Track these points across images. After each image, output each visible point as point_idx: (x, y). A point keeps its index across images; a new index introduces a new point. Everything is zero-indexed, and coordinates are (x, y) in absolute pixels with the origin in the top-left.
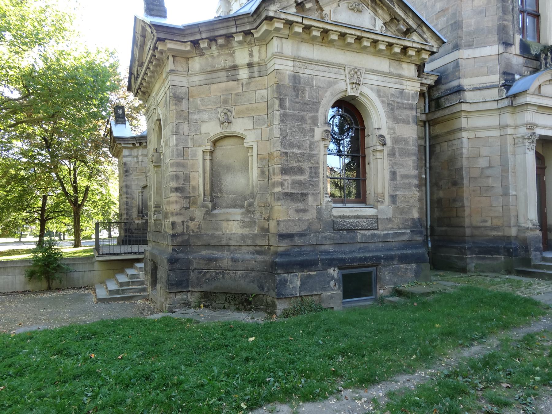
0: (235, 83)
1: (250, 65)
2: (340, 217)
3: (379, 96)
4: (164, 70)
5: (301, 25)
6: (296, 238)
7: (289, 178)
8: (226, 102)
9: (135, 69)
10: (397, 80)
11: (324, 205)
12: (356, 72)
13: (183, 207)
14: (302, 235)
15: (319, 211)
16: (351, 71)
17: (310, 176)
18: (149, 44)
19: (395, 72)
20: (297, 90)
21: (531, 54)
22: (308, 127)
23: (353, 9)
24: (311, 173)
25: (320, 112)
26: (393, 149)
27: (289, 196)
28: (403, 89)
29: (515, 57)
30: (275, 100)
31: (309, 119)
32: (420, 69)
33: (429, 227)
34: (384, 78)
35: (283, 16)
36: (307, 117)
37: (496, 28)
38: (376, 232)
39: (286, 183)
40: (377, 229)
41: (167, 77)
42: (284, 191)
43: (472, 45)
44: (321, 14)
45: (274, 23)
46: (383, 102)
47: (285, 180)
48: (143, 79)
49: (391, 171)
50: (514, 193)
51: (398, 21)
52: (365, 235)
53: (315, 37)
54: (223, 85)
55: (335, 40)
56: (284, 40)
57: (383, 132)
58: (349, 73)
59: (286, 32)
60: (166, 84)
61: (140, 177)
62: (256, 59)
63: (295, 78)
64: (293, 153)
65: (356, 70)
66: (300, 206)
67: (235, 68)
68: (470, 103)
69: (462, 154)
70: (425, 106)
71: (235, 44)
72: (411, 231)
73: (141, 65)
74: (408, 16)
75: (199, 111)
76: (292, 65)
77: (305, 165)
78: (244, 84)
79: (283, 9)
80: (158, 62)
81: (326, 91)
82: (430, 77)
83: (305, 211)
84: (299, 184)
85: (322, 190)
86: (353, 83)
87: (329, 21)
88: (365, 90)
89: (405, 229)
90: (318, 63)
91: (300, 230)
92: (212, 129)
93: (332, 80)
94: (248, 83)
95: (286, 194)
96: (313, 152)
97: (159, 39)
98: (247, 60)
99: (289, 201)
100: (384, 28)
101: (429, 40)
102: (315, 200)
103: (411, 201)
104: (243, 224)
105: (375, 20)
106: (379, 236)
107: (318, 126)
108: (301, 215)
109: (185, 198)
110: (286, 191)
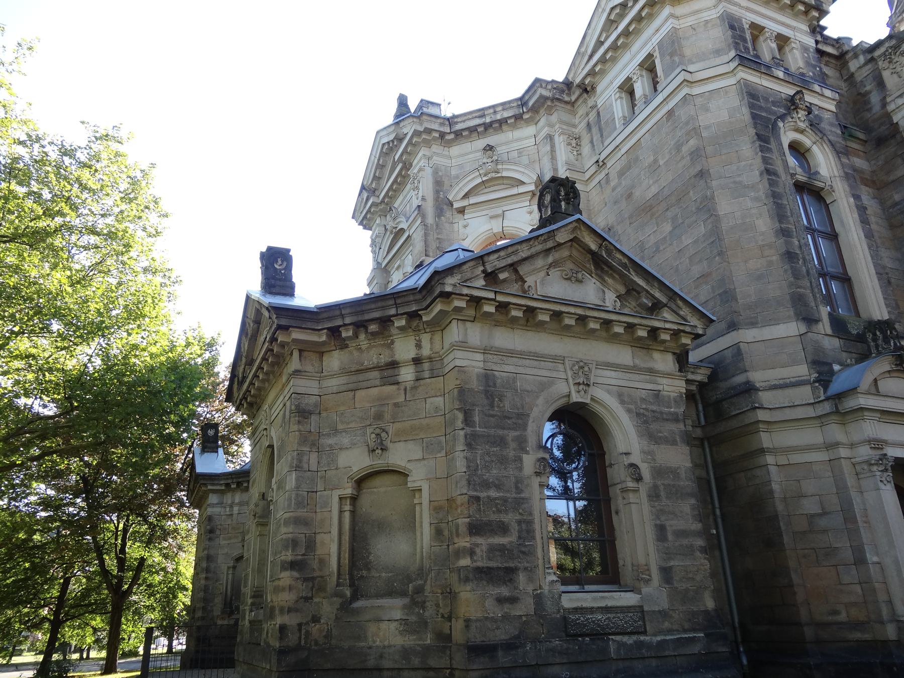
0: (394, 387)
1: (417, 361)
2: (576, 610)
3: (622, 402)
4: (285, 370)
6: (500, 653)
7: (483, 542)
8: (379, 416)
9: (241, 369)
11: (546, 588)
12: (582, 368)
13: (302, 598)
14: (510, 646)
15: (539, 599)
16: (574, 365)
17: (520, 538)
19: (643, 365)
20: (491, 396)
21: (850, 333)
22: (512, 454)
24: (520, 532)
25: (530, 429)
26: (655, 487)
27: (484, 575)
29: (827, 338)
30: (457, 412)
31: (512, 440)
32: (682, 359)
33: (737, 625)
34: (628, 375)
35: (466, 291)
36: (509, 439)
37: (788, 297)
38: (642, 638)
39: (478, 550)
40: (645, 633)
41: (288, 381)
42: (475, 564)
43: (757, 323)
45: (452, 300)
46: (629, 411)
47: (477, 545)
48: (251, 383)
49: (656, 525)
50: (875, 559)
51: (639, 293)
52: (624, 644)
54: (374, 391)
55: (545, 322)
56: (468, 324)
57: (635, 458)
58: (571, 369)
59: (472, 312)
61: (233, 541)
62: (426, 352)
63: (488, 378)
64: (489, 497)
65: (582, 364)
66: (505, 591)
67: (394, 365)
68: (770, 409)
69: (771, 492)
70: (698, 415)
71: (394, 331)
72: (707, 635)
73: (250, 363)
74: (652, 286)
75: (336, 431)
77: (510, 518)
78: (408, 388)
79: (465, 281)
81: (538, 397)
83: (513, 600)
84: (500, 551)
85: (540, 562)
86: (579, 384)
88: (600, 393)
89: (694, 630)
91: (507, 637)
92: (355, 460)
94: (414, 388)
95: (479, 570)
96: (522, 495)
97: (280, 327)
98: (412, 353)
99: (485, 583)
100: (618, 304)
101: (688, 318)
102: (531, 580)
103: (699, 578)
104: (407, 627)
105: (604, 292)
106: (649, 646)
107: (527, 453)
108: (507, 608)
109: (306, 580)
110: (480, 564)
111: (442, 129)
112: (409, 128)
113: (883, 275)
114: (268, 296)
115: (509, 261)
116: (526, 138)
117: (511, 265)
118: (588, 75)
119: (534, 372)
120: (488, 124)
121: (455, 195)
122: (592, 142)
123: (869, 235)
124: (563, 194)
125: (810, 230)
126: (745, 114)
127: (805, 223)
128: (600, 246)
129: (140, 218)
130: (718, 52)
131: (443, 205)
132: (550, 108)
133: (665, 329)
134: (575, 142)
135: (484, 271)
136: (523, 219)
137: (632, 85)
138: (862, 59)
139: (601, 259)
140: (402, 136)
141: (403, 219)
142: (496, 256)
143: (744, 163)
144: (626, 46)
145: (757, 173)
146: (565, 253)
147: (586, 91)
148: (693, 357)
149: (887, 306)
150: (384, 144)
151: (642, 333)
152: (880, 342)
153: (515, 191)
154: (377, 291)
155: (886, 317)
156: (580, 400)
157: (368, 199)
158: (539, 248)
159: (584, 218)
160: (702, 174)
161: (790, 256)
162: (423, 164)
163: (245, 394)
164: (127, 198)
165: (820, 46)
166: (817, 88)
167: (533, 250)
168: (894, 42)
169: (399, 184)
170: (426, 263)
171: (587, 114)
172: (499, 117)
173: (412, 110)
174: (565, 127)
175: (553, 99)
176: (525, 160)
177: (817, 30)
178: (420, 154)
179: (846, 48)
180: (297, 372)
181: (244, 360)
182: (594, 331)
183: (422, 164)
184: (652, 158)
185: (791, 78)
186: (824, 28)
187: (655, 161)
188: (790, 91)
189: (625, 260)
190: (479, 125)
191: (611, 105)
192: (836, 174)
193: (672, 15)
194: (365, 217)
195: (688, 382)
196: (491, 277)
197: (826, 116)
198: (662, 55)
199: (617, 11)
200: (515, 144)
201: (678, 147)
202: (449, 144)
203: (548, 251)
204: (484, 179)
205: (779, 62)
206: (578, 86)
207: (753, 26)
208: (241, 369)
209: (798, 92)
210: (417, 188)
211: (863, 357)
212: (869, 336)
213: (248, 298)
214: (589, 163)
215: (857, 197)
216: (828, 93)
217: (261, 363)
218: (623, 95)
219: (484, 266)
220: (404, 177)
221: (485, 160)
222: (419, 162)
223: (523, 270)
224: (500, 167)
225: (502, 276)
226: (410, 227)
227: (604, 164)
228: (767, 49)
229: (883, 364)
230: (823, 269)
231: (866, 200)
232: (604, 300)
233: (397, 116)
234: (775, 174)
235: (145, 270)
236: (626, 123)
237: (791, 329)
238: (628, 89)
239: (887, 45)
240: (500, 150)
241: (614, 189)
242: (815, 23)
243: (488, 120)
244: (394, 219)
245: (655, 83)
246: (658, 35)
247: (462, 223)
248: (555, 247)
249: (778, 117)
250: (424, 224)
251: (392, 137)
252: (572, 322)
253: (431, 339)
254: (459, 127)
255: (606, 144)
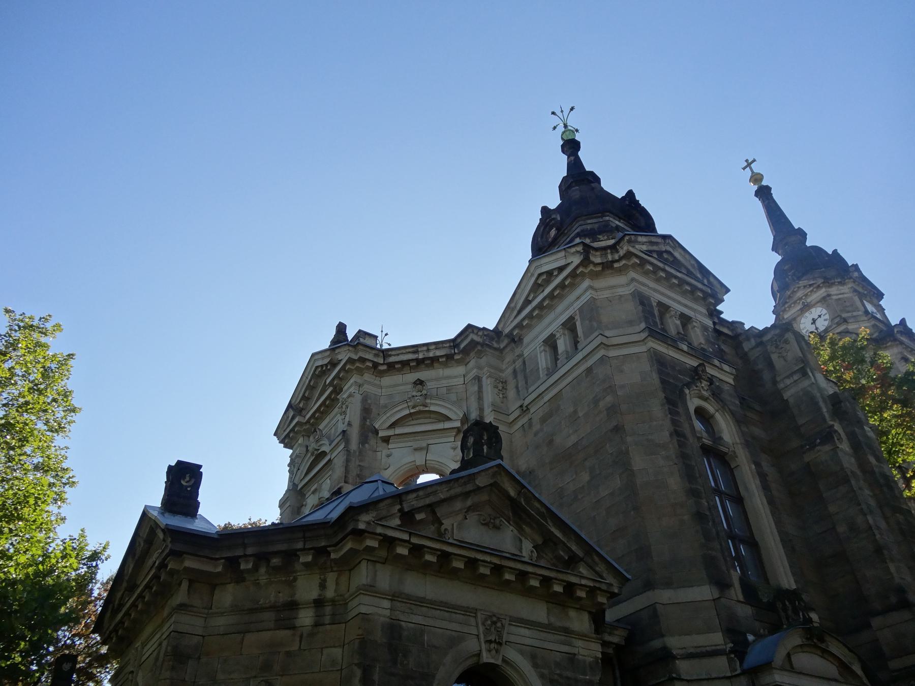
0: (288, 633)
1: (319, 603)
3: (535, 666)
4: (169, 602)
5: (407, 544)
8: (266, 667)
9: (119, 595)
10: (563, 638)
12: (494, 623)
16: (486, 620)
18: (156, 555)
19: (558, 624)
23: (486, 524)
28: (575, 654)
30: (355, 668)
32: (598, 619)
35: (379, 530)
41: (170, 615)
44: (439, 529)
46: (542, 676)
48: (127, 614)
53: (429, 563)
54: (266, 636)
55: (460, 569)
56: (378, 566)
58: (483, 624)
59: (383, 553)
60: (165, 629)
62: (330, 593)
63: (393, 629)
65: (495, 619)
67: (293, 606)
68: (688, 681)
71: (298, 567)
73: (132, 588)
76: (389, 606)
78: (305, 635)
79: (380, 519)
80: (162, 589)
82: (616, 632)
86: (490, 642)
87: (451, 541)
88: (512, 654)
90: (435, 604)
93: (453, 633)
94: (312, 635)
97: (173, 553)
98: (314, 594)
100: (535, 554)
105: (521, 541)
111: (375, 360)
112: (344, 355)
113: (786, 540)
114: (167, 515)
115: (428, 501)
116: (456, 377)
117: (429, 506)
118: (515, 328)
119: (444, 624)
120: (420, 358)
121: (381, 423)
122: (517, 387)
123: (771, 502)
124: (485, 438)
125: (717, 491)
126: (655, 379)
127: (713, 484)
128: (519, 493)
129: (45, 411)
130: (631, 323)
131: (368, 432)
132: (480, 352)
133: (581, 585)
134: (502, 385)
135: (400, 510)
136: (449, 454)
137: (555, 342)
138: (753, 342)
139: (518, 506)
140: (336, 362)
141: (326, 442)
142: (414, 495)
143: (655, 423)
144: (551, 307)
145: (667, 434)
146: (484, 497)
147: (513, 341)
148: (610, 616)
149: (794, 574)
150: (317, 367)
151: (558, 588)
152: (790, 612)
153: (440, 426)
154: (286, 522)
155: (794, 587)
156: (492, 661)
157: (293, 418)
158: (458, 490)
159: (506, 463)
160: (618, 429)
161: (700, 517)
162: (353, 390)
163: (117, 625)
164: (35, 389)
165: (717, 327)
166: (716, 362)
167: (452, 492)
168: (777, 331)
169: (327, 407)
170: (344, 491)
171: (514, 362)
172: (431, 354)
173: (350, 338)
174: (492, 371)
175: (483, 345)
176: (453, 397)
177: (715, 314)
178: (352, 381)
179: (739, 331)
180: (182, 607)
181: (125, 585)
182: (508, 582)
183: (352, 390)
184: (572, 409)
185: (694, 351)
186: (721, 313)
187: (575, 412)
188: (694, 363)
189: (543, 510)
190: (412, 360)
191: (536, 356)
192: (738, 441)
193: (591, 287)
194: (287, 436)
195: (605, 644)
196: (407, 517)
197: (726, 387)
198: (582, 319)
199: (544, 277)
200: (444, 381)
201: (596, 401)
202: (381, 374)
203: (467, 495)
204: (412, 411)
205: (684, 337)
206: (507, 336)
207: (660, 304)
208: (119, 595)
209: (700, 365)
210: (345, 413)
211: (775, 628)
212: (779, 605)
213: (145, 515)
214: (514, 406)
215: (758, 464)
216: (726, 367)
217: (143, 591)
218: (547, 349)
219: (401, 504)
220: (333, 400)
221: (414, 394)
222: (350, 387)
223: (440, 512)
224: (428, 401)
225: (419, 517)
226: (332, 450)
227: (528, 409)
228: (673, 325)
229: (794, 639)
230: (731, 531)
231: (766, 467)
232: (521, 550)
233: (334, 342)
234: (684, 436)
235: (37, 468)
236: (550, 374)
237: (704, 592)
238: (551, 343)
239: (773, 332)
240: (430, 385)
241: (536, 434)
242: (712, 307)
243: (421, 356)
244: (317, 441)
245: (576, 343)
246: (578, 302)
247: (385, 452)
248: (474, 491)
249: (684, 385)
250: (347, 450)
251: (326, 361)
252: (487, 571)
253: (337, 579)
254: (392, 359)
255: (531, 390)
